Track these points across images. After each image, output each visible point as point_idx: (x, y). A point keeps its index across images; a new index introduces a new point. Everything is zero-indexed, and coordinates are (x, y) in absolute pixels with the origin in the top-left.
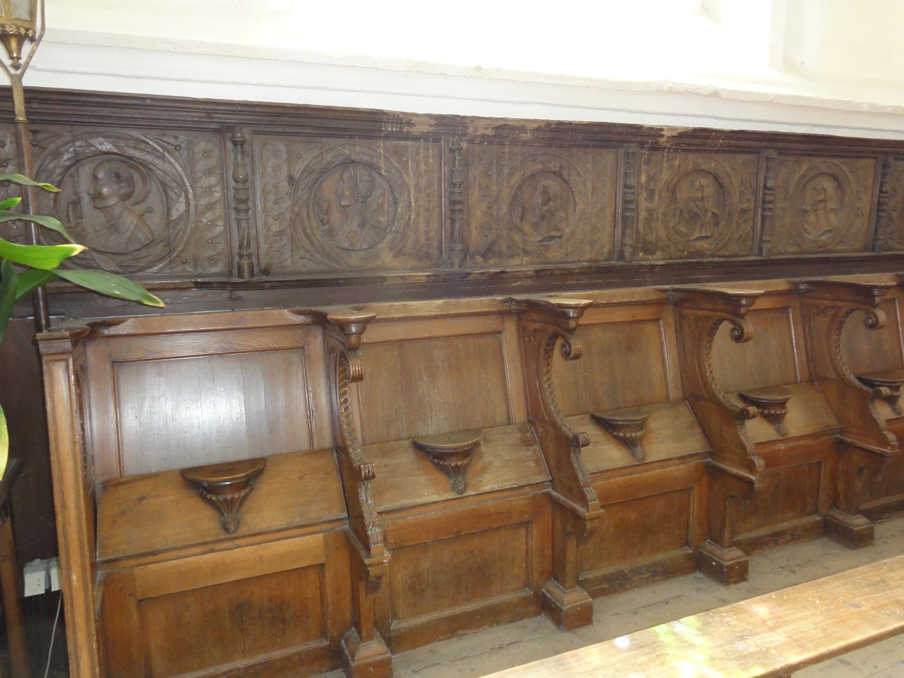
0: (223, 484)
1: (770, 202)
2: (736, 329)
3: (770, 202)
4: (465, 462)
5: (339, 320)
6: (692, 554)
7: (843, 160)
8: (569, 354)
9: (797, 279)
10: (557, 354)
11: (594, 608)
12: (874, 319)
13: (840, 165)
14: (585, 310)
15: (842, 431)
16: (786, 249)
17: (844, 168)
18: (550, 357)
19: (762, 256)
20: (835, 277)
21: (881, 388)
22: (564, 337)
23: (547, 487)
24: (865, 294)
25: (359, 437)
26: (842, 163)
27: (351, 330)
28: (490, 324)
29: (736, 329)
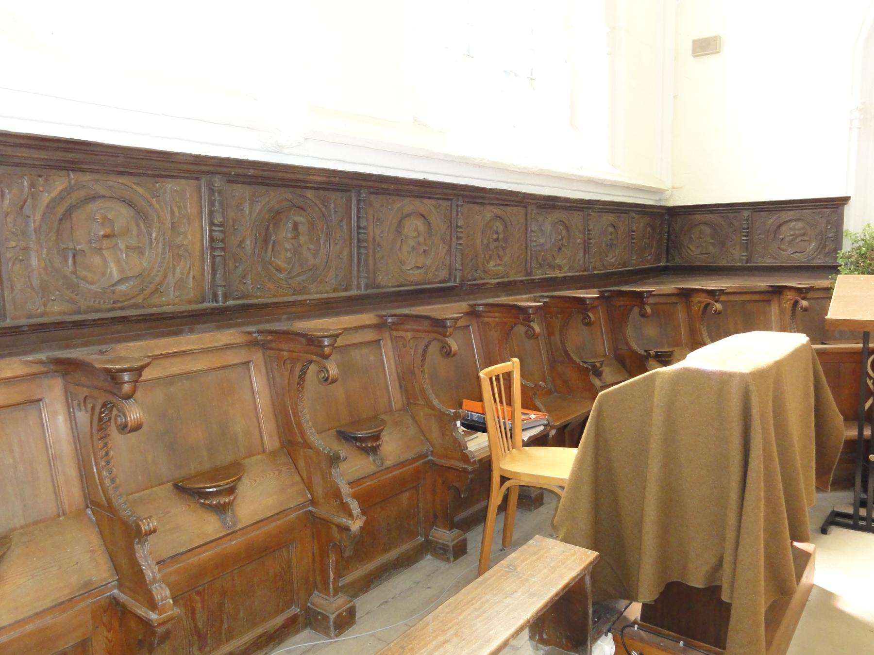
0: (207, 490)
1: (364, 228)
2: (322, 370)
3: (364, 228)
4: (232, 498)
5: (108, 368)
6: (425, 540)
7: (136, 179)
8: (327, 380)
9: (384, 313)
10: (113, 430)
11: (468, 540)
12: (448, 348)
13: (134, 187)
14: (338, 337)
15: (313, 502)
16: (388, 280)
17: (140, 190)
18: (106, 436)
19: (361, 290)
20: (419, 308)
21: (651, 352)
22: (318, 363)
23: (308, 507)
24: (439, 325)
25: (394, 409)
26: (134, 183)
27: (123, 378)
28: (369, 336)
29: (322, 370)
